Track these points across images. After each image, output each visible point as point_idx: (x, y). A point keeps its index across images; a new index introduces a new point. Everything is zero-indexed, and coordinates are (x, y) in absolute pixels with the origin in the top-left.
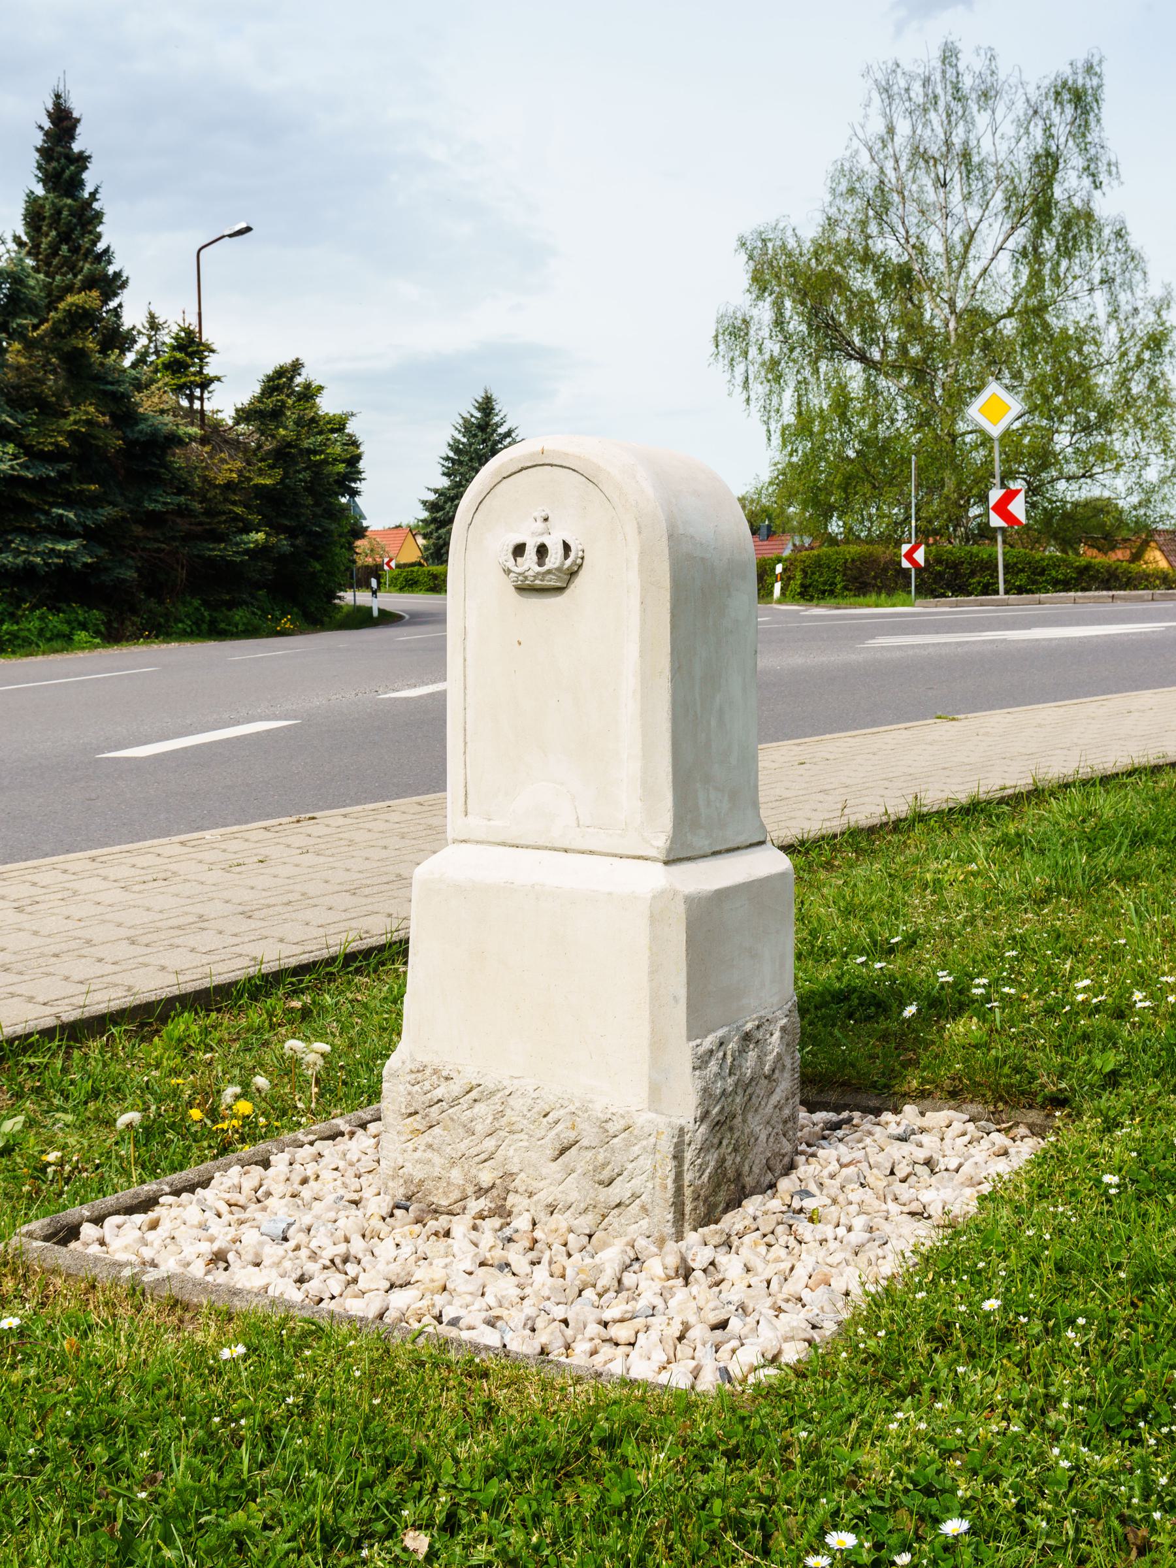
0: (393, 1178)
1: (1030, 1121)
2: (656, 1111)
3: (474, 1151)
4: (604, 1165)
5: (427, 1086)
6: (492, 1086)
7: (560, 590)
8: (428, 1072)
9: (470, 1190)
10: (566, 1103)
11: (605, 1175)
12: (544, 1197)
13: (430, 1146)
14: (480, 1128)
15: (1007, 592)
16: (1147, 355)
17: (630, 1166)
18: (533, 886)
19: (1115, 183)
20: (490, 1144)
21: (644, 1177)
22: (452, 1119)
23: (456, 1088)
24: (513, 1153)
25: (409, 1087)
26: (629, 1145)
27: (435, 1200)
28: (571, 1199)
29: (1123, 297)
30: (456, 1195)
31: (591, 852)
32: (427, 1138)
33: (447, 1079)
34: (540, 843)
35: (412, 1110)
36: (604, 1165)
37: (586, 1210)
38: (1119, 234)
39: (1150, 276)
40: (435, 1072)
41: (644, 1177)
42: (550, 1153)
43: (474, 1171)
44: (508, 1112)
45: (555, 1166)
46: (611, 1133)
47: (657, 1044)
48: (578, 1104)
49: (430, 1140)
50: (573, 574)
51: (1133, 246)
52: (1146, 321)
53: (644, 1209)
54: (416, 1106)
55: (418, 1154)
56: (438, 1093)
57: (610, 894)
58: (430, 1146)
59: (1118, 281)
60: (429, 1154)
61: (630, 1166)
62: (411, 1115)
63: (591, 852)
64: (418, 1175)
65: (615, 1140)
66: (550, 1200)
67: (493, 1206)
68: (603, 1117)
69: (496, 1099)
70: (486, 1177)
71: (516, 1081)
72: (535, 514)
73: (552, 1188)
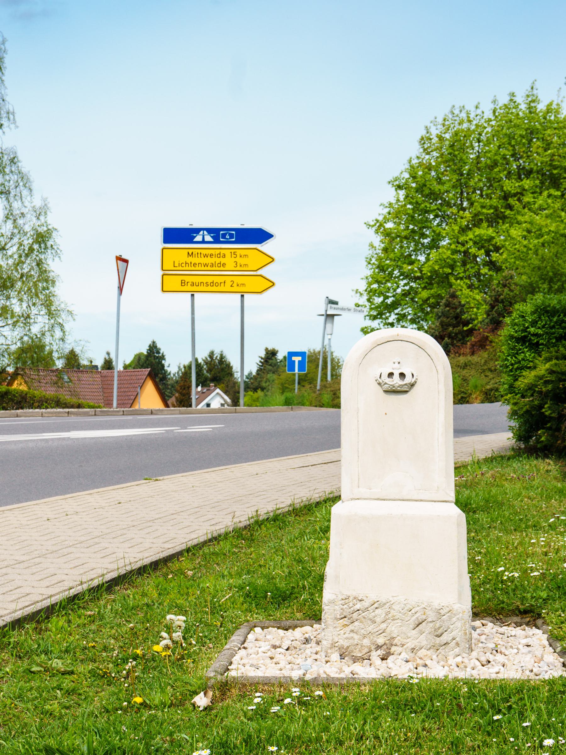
0: (331, 648)
1: (515, 621)
2: (460, 604)
3: (375, 630)
4: (439, 628)
5: (351, 605)
6: (384, 601)
7: (406, 392)
8: (351, 599)
9: (373, 647)
10: (420, 604)
11: (440, 631)
12: (410, 645)
13: (352, 631)
14: (378, 620)
15: (244, 405)
16: (36, 246)
17: (451, 627)
18: (402, 515)
19: (12, 126)
20: (383, 626)
21: (457, 631)
22: (364, 618)
23: (366, 604)
24: (393, 629)
25: (342, 606)
26: (450, 618)
27: (355, 654)
28: (422, 645)
29: (16, 205)
30: (366, 650)
31: (421, 500)
32: (351, 627)
33: (361, 601)
34: (397, 498)
35: (343, 616)
36: (439, 628)
37: (430, 648)
38: (13, 161)
39: (34, 192)
40: (355, 598)
41: (457, 631)
42: (412, 627)
43: (375, 639)
44: (392, 611)
45: (414, 632)
46: (442, 614)
47: (460, 576)
48: (426, 604)
49: (353, 628)
50: (412, 385)
51: (24, 170)
52: (29, 224)
53: (458, 644)
54: (345, 614)
55: (346, 635)
56: (358, 607)
57: (438, 516)
58: (352, 631)
59: (13, 193)
60: (352, 635)
61: (451, 627)
62: (342, 618)
63: (421, 500)
64: (346, 644)
65: (444, 617)
66: (413, 646)
67: (384, 653)
68: (439, 608)
69: (387, 606)
70: (381, 641)
71: (395, 598)
72: (394, 361)
73: (413, 641)
